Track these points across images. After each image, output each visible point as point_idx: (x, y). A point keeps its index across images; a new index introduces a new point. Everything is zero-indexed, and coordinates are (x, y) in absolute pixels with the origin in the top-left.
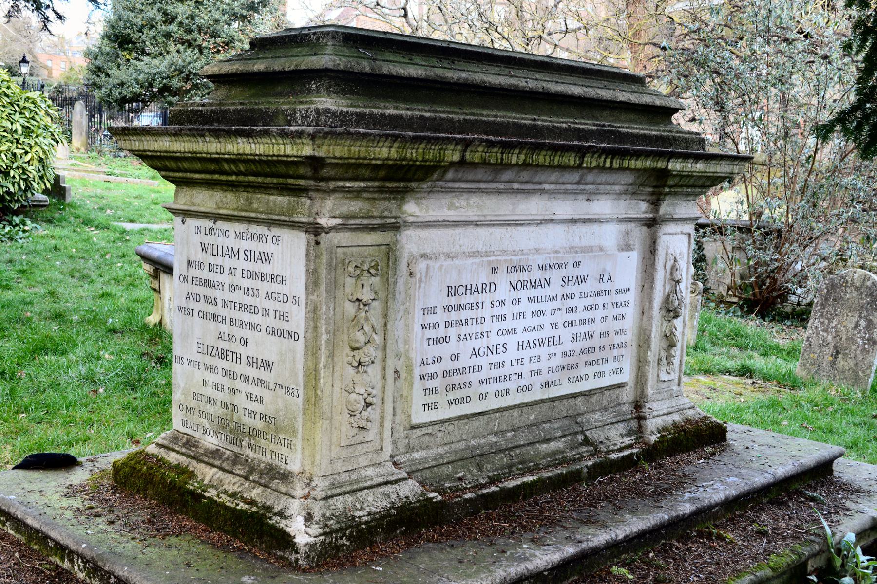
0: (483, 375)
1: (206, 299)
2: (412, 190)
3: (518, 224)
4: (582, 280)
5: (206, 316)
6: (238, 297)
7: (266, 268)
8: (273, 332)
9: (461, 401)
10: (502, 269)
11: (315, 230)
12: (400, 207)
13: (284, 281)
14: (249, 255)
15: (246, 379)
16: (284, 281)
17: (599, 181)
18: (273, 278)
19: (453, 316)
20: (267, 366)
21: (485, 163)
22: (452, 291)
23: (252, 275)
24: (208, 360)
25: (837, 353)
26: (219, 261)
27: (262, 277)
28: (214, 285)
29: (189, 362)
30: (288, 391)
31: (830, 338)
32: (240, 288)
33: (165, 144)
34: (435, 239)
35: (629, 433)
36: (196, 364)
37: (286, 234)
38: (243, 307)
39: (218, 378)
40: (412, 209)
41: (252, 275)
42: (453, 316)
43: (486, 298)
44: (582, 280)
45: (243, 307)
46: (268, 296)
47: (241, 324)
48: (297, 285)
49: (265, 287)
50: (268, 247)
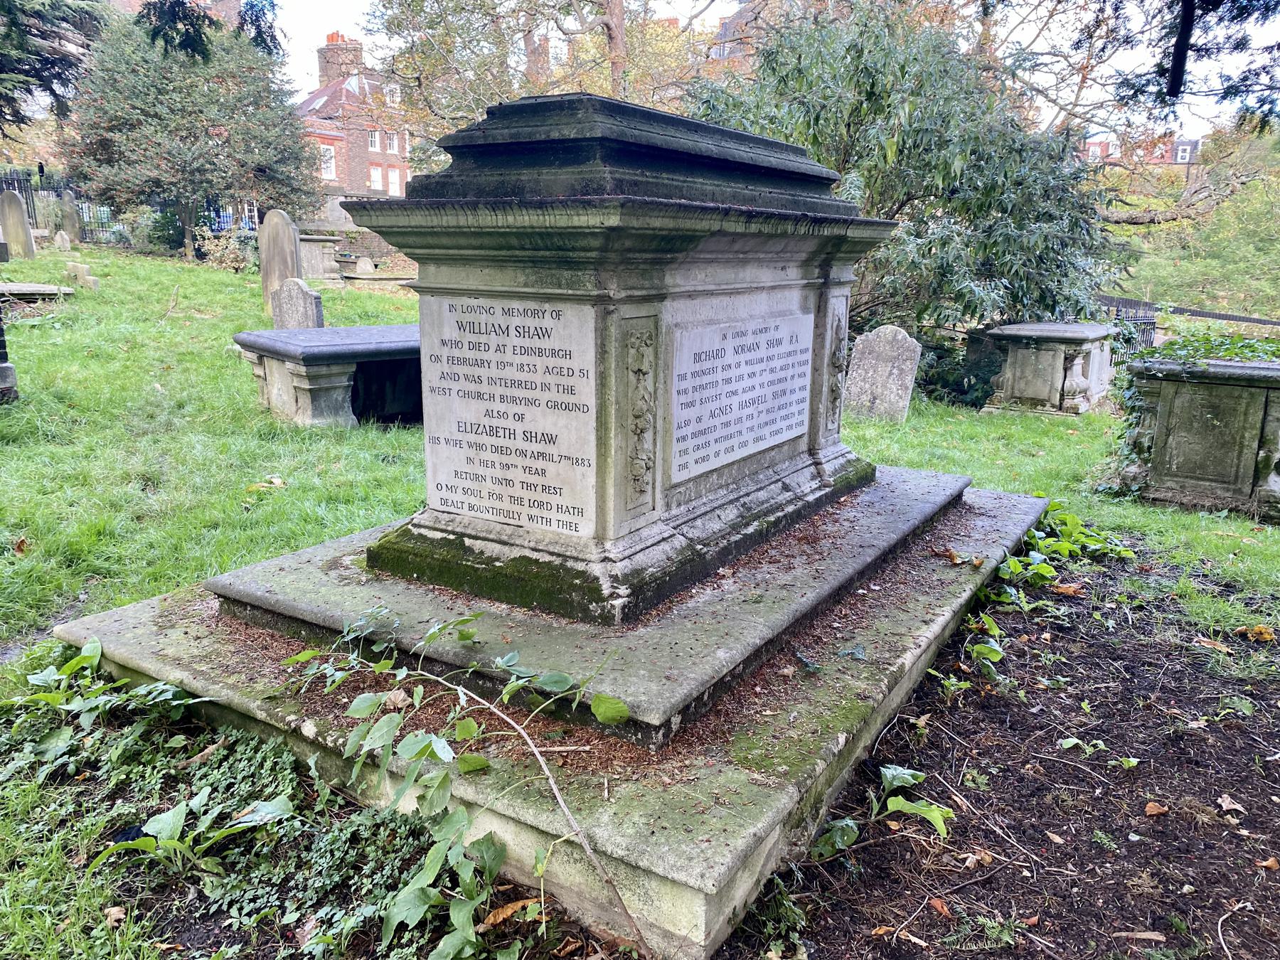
0: (716, 435)
1: (466, 378)
2: (672, 261)
3: (737, 292)
4: (779, 342)
5: (467, 395)
6: (510, 373)
7: (545, 344)
8: (556, 406)
9: (704, 459)
10: (729, 336)
11: (602, 302)
12: (662, 279)
13: (568, 355)
14: (522, 332)
15: (523, 453)
16: (568, 355)
17: (747, 249)
18: (554, 353)
19: (698, 381)
20: (551, 440)
21: (760, 234)
22: (697, 358)
23: (526, 351)
24: (472, 438)
25: (875, 398)
26: (483, 339)
27: (540, 352)
28: (480, 363)
29: (447, 441)
30: (577, 462)
31: (867, 386)
32: (512, 365)
33: (419, 219)
34: (705, 309)
35: (813, 478)
36: (457, 443)
37: (569, 311)
38: (519, 384)
39: (487, 455)
40: (676, 280)
41: (526, 351)
42: (698, 381)
43: (718, 363)
44: (779, 342)
45: (519, 384)
46: (548, 370)
47: (514, 400)
48: (586, 357)
49: (540, 362)
50: (548, 322)
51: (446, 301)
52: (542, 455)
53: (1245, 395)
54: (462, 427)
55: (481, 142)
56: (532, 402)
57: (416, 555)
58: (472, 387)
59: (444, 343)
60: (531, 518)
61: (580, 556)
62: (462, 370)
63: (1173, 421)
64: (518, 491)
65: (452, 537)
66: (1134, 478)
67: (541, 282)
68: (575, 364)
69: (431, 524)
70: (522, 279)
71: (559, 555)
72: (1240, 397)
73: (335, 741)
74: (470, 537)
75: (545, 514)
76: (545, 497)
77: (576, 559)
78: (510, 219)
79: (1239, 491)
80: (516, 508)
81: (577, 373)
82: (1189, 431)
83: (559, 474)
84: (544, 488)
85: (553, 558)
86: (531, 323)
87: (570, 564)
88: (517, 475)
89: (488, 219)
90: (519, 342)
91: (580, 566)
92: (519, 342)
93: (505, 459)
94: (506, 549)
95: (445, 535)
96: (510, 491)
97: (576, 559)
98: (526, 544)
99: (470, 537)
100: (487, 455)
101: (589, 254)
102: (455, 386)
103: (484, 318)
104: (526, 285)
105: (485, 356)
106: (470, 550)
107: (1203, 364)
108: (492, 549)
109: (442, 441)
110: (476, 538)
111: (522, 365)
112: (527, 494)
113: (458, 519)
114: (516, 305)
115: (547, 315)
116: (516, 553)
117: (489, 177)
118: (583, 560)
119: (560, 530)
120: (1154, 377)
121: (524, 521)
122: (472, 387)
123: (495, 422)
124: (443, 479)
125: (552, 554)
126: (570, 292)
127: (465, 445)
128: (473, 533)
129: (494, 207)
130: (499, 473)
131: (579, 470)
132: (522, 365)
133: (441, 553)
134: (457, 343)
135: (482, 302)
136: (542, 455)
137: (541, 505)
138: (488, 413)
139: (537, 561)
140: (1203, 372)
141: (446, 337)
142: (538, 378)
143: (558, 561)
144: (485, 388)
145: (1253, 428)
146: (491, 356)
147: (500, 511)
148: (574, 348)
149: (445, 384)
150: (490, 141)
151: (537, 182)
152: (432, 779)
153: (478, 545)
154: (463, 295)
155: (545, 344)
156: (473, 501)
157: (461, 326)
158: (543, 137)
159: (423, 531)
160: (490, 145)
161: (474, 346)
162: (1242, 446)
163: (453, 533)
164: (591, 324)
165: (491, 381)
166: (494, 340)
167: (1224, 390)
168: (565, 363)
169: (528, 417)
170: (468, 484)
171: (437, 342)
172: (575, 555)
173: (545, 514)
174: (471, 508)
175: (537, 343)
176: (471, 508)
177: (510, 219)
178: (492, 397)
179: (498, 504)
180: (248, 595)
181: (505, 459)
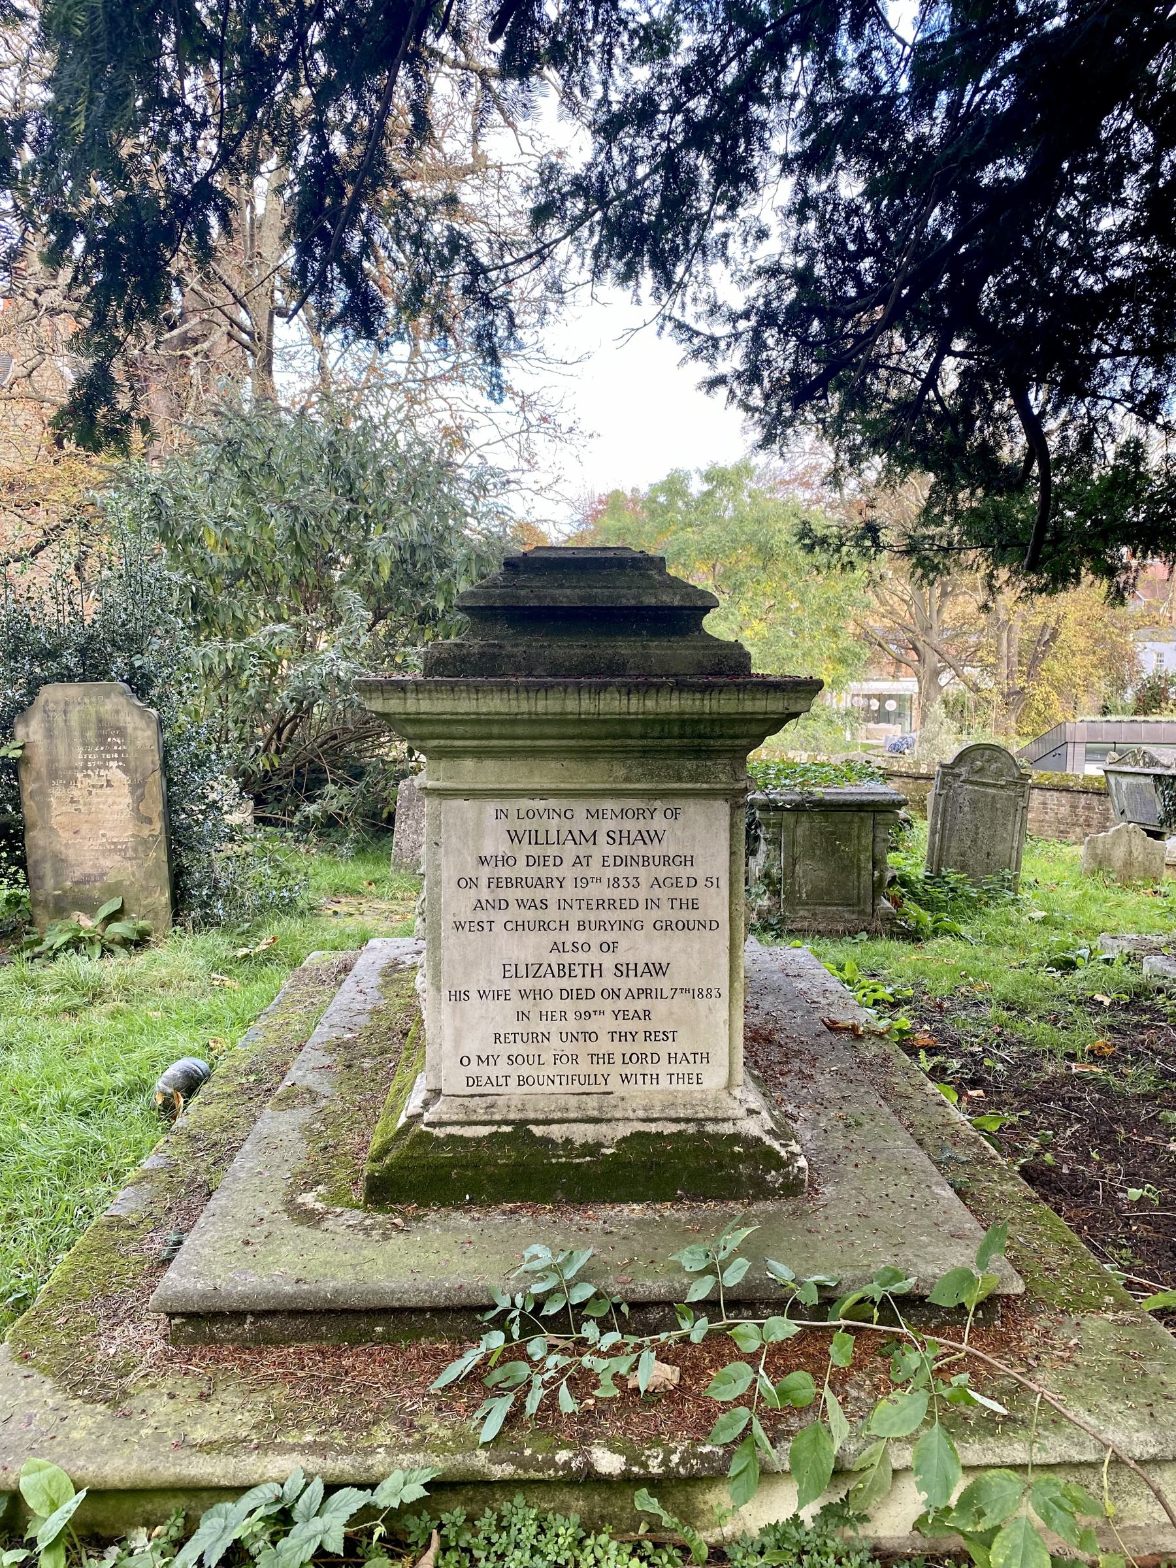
6: (595, 891)
8: (668, 926)
15: (615, 994)
18: (666, 860)
20: (659, 970)
23: (622, 861)
24: (527, 984)
26: (552, 851)
27: (646, 861)
29: (482, 994)
37: (692, 810)
41: (622, 861)
47: (601, 925)
50: (658, 823)
51: (490, 807)
52: (645, 992)
53: (856, 819)
54: (510, 971)
55: (533, 603)
56: (625, 925)
57: (466, 1167)
58: (531, 915)
59: (482, 861)
60: (625, 1079)
61: (720, 1115)
62: (512, 894)
63: (798, 850)
64: (604, 1045)
65: (507, 1129)
66: (769, 912)
67: (652, 775)
68: (699, 872)
69: (462, 1117)
70: (621, 772)
71: (688, 1120)
72: (852, 822)
73: (665, 1462)
74: (537, 1122)
75: (650, 1069)
76: (649, 1047)
77: (716, 1120)
78: (650, 704)
79: (862, 912)
80: (602, 1069)
81: (701, 882)
82: (812, 858)
83: (672, 1013)
84: (648, 1035)
85: (682, 1126)
86: (632, 826)
87: (710, 1128)
88: (603, 1024)
89: (612, 704)
90: (611, 850)
91: (727, 1129)
92: (611, 850)
93: (583, 1006)
94: (603, 1128)
95: (494, 1129)
96: (592, 1047)
97: (716, 1120)
98: (631, 1115)
99: (537, 1122)
100: (554, 1005)
101: (737, 742)
102: (500, 917)
103: (554, 823)
104: (627, 779)
105: (555, 872)
106: (547, 1141)
107: (819, 792)
108: (583, 1133)
109: (474, 995)
110: (548, 1122)
111: (616, 880)
112: (618, 1048)
113: (501, 1101)
114: (609, 804)
115: (658, 815)
116: (623, 1130)
117: (518, 645)
118: (724, 1120)
119: (674, 1086)
120: (782, 809)
121: (615, 1084)
122: (531, 915)
123: (567, 958)
124: (472, 1048)
125: (677, 1120)
126: (705, 786)
127: (513, 995)
128: (541, 1117)
129: (629, 690)
130: (572, 1025)
131: (703, 1003)
132: (616, 880)
133: (506, 1156)
134: (505, 860)
135: (552, 803)
136: (645, 992)
137: (642, 1058)
138: (556, 947)
139: (659, 1135)
140: (821, 800)
141: (488, 852)
142: (641, 894)
143: (691, 1129)
144: (552, 914)
145: (866, 850)
146: (566, 871)
147: (572, 1079)
148: (698, 852)
149: (482, 916)
150: (547, 602)
151: (646, 657)
152: (871, 1456)
153: (557, 1132)
154: (523, 796)
155: (654, 850)
156: (525, 1070)
157: (514, 836)
158: (633, 602)
159: (450, 1130)
160: (548, 608)
161: (531, 861)
162: (859, 870)
163: (507, 1122)
164: (725, 822)
165: (563, 904)
166: (570, 851)
167: (837, 817)
168: (685, 872)
169: (622, 946)
170: (518, 1048)
171: (471, 861)
172: (712, 1114)
173: (650, 1069)
174: (523, 1081)
175: (640, 849)
176: (523, 1081)
177: (650, 704)
178: (564, 925)
179: (568, 1069)
180: (267, 1298)
181: (583, 1006)
